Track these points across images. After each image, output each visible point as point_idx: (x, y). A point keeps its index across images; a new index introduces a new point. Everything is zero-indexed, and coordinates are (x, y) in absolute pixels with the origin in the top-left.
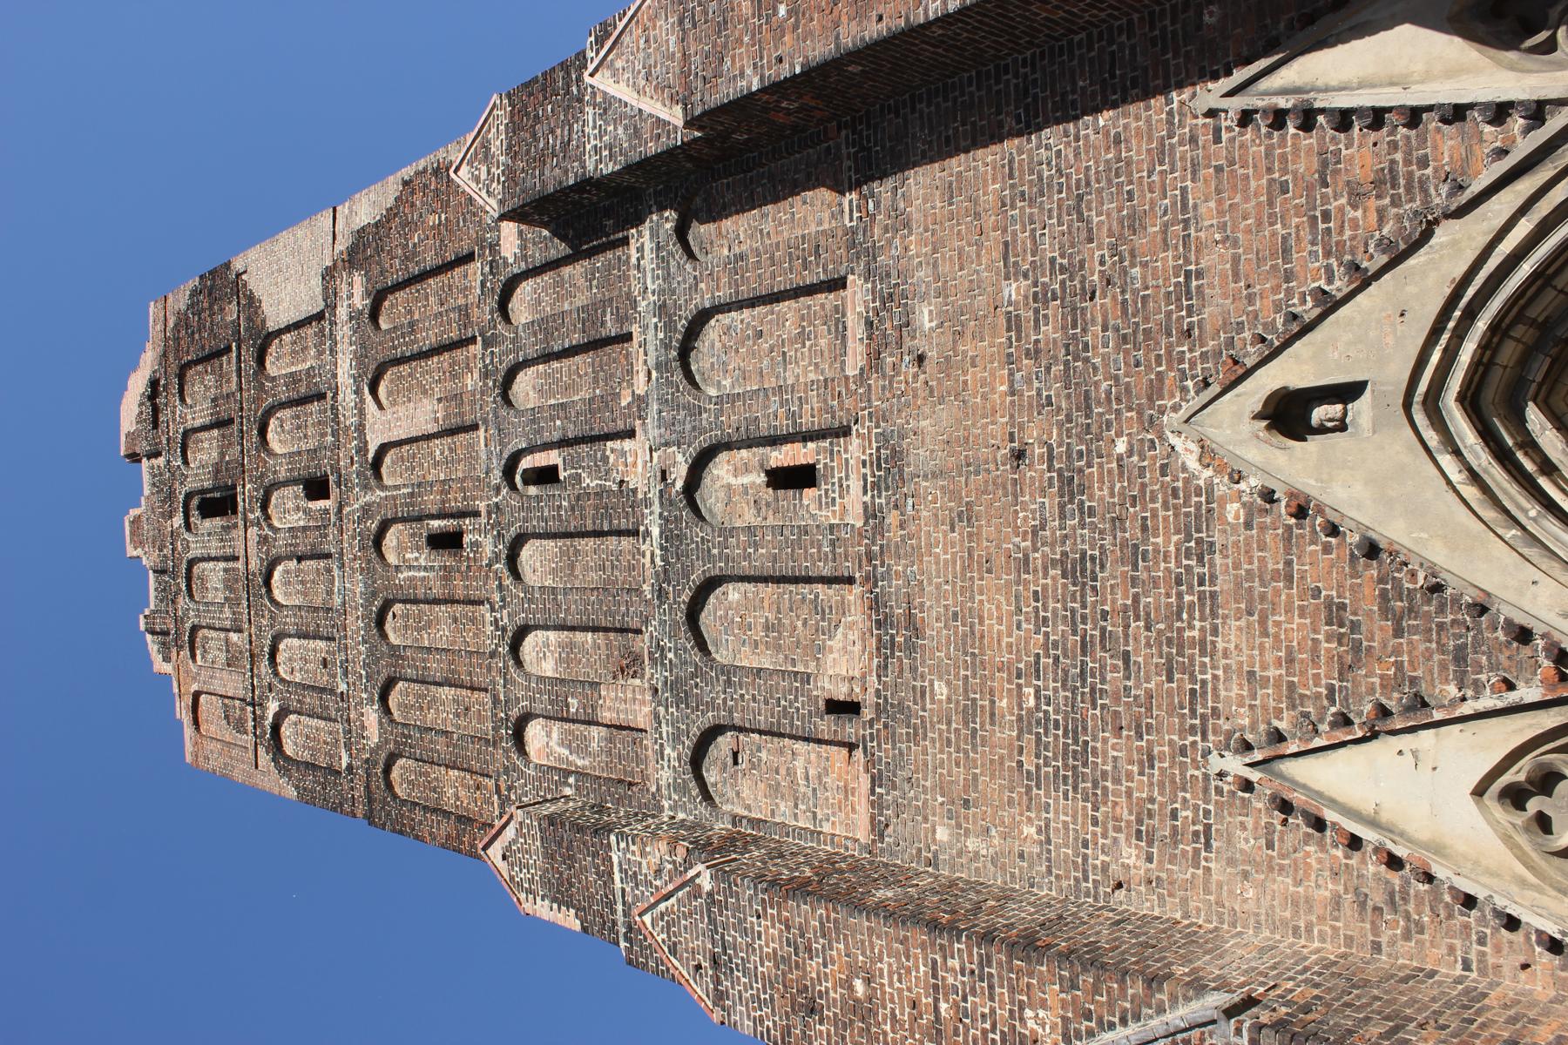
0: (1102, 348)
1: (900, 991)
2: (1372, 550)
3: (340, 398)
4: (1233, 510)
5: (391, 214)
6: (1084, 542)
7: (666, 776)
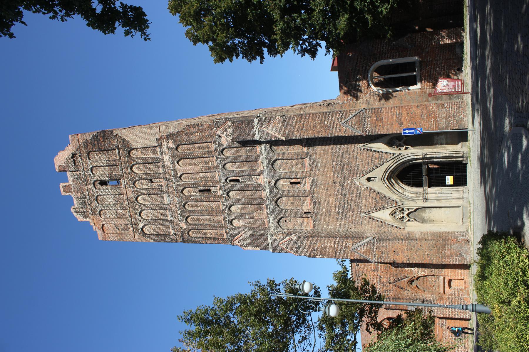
0: (346, 171)
2: (379, 193)
3: (165, 163)
4: (363, 189)
6: (345, 192)
7: (271, 225)
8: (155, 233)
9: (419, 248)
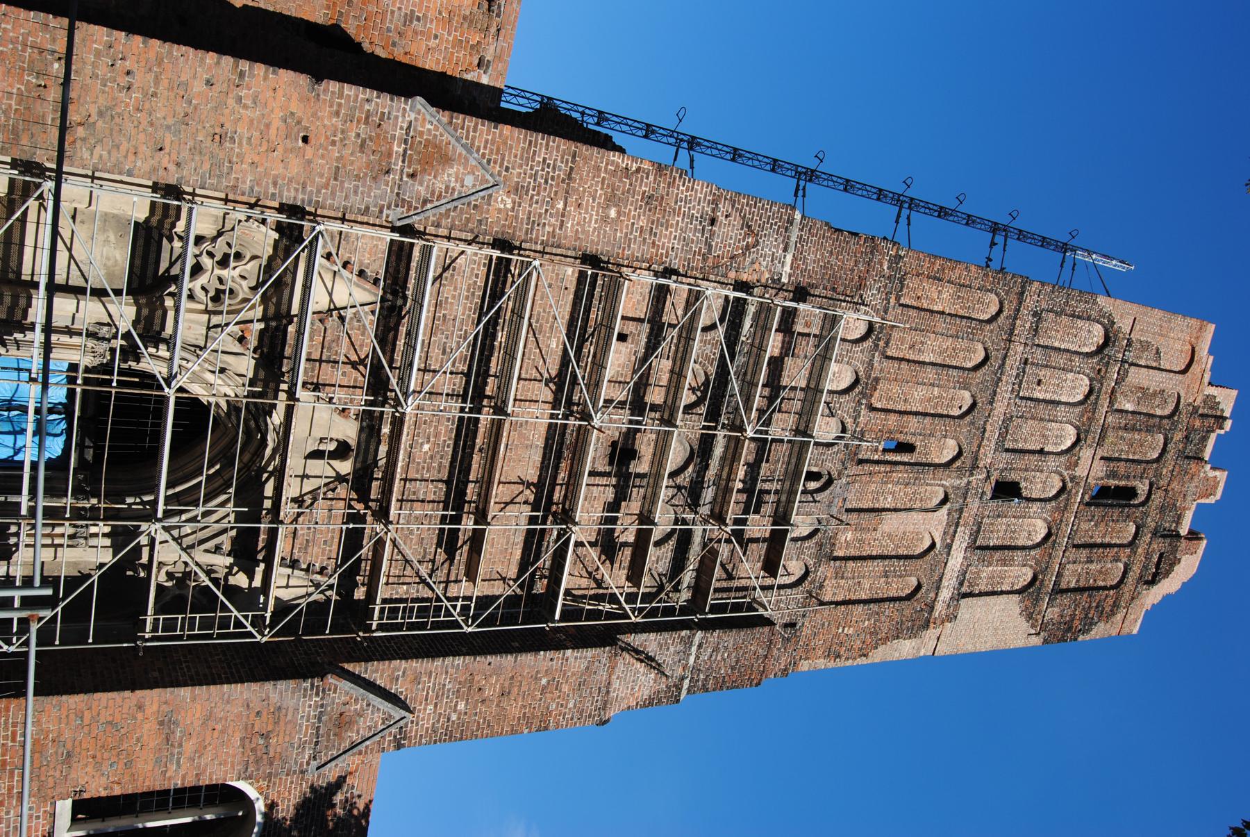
1: (587, 213)
5: (885, 640)
8: (1080, 323)
9: (169, 138)
